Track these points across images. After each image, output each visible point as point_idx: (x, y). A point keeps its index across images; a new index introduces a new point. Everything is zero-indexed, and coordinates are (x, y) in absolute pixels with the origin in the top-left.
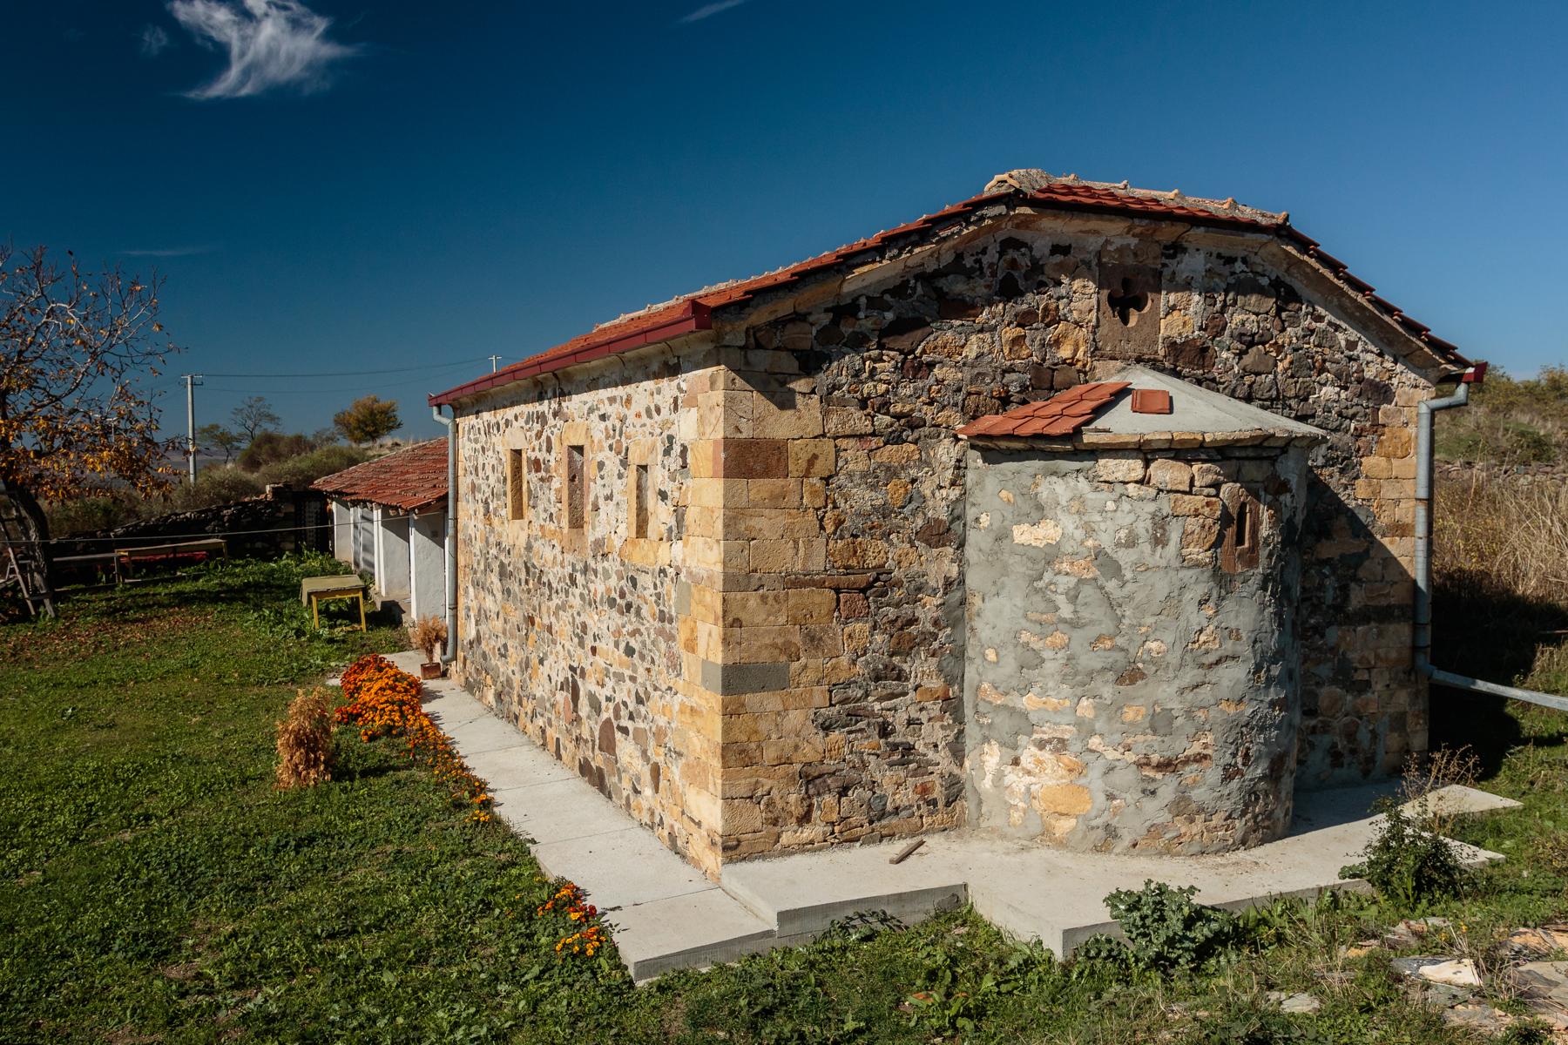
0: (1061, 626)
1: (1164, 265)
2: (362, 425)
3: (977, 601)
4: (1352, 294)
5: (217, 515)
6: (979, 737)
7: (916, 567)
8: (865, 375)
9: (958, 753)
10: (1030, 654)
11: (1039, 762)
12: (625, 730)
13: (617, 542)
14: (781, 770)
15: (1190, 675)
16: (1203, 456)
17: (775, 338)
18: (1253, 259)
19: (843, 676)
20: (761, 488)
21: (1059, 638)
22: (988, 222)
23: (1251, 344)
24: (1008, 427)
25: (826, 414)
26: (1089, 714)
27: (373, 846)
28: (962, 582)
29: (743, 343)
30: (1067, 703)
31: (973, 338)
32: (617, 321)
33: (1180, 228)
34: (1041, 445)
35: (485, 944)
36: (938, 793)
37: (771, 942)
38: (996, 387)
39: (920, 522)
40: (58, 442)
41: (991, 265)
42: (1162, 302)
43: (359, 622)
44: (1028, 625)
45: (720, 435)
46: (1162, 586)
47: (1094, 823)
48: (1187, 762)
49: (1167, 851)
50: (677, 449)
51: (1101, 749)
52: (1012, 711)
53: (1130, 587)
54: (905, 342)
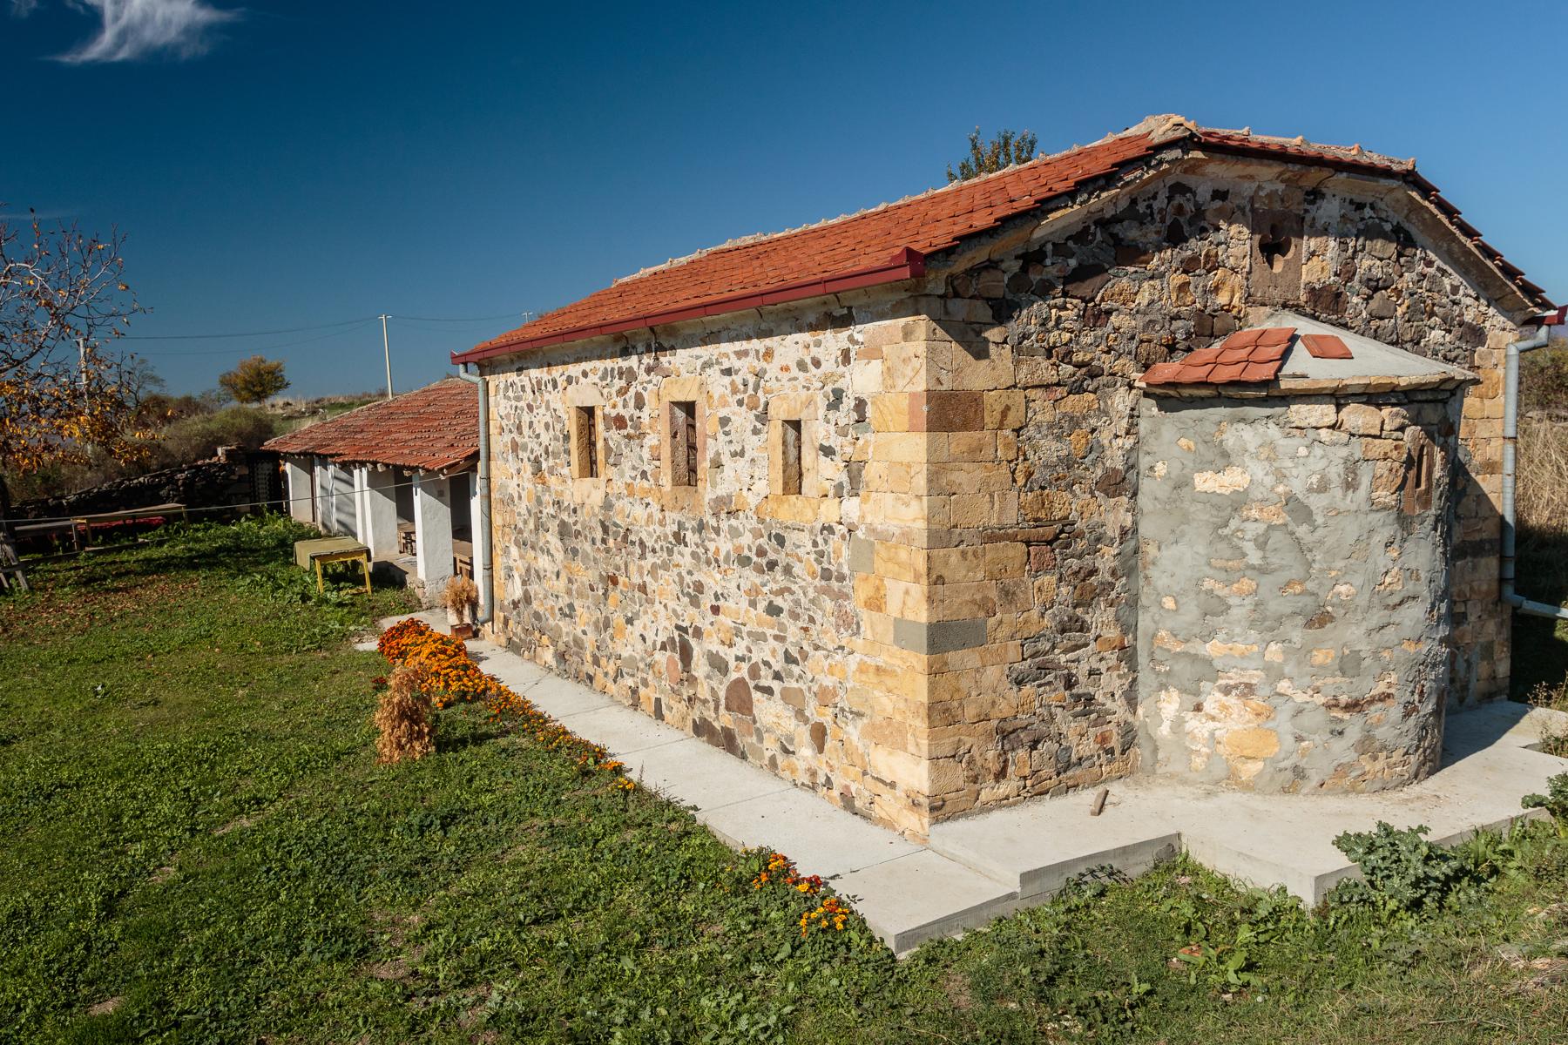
0: (1249, 572)
1: (1306, 211)
2: (249, 385)
3: (1151, 550)
4: (1463, 239)
5: (171, 480)
6: (1155, 684)
7: (1096, 518)
8: (1052, 323)
9: (1132, 702)
10: (1215, 601)
11: (1225, 707)
12: (769, 691)
13: (752, 500)
14: (981, 727)
15: (1376, 617)
16: (1394, 400)
17: (972, 281)
18: (1381, 205)
19: (1034, 630)
20: (961, 440)
21: (1247, 584)
22: (1165, 166)
23: (1376, 289)
24: (1200, 374)
25: (1017, 363)
26: (1278, 659)
27: (519, 821)
28: (1136, 531)
29: (941, 292)
30: (1255, 648)
31: (1146, 285)
32: (637, 276)
33: (1326, 172)
34: (1232, 392)
35: (710, 921)
36: (1115, 742)
37: (1015, 904)
38: (1165, 335)
39: (1099, 472)
40: (26, 407)
41: (1160, 211)
42: (1304, 248)
43: (364, 584)
44: (1211, 572)
45: (921, 386)
46: (1352, 530)
47: (1282, 765)
48: (1372, 701)
49: (1352, 790)
50: (848, 403)
51: (1289, 692)
52: (1194, 658)
53: (1320, 532)
54: (1085, 289)
